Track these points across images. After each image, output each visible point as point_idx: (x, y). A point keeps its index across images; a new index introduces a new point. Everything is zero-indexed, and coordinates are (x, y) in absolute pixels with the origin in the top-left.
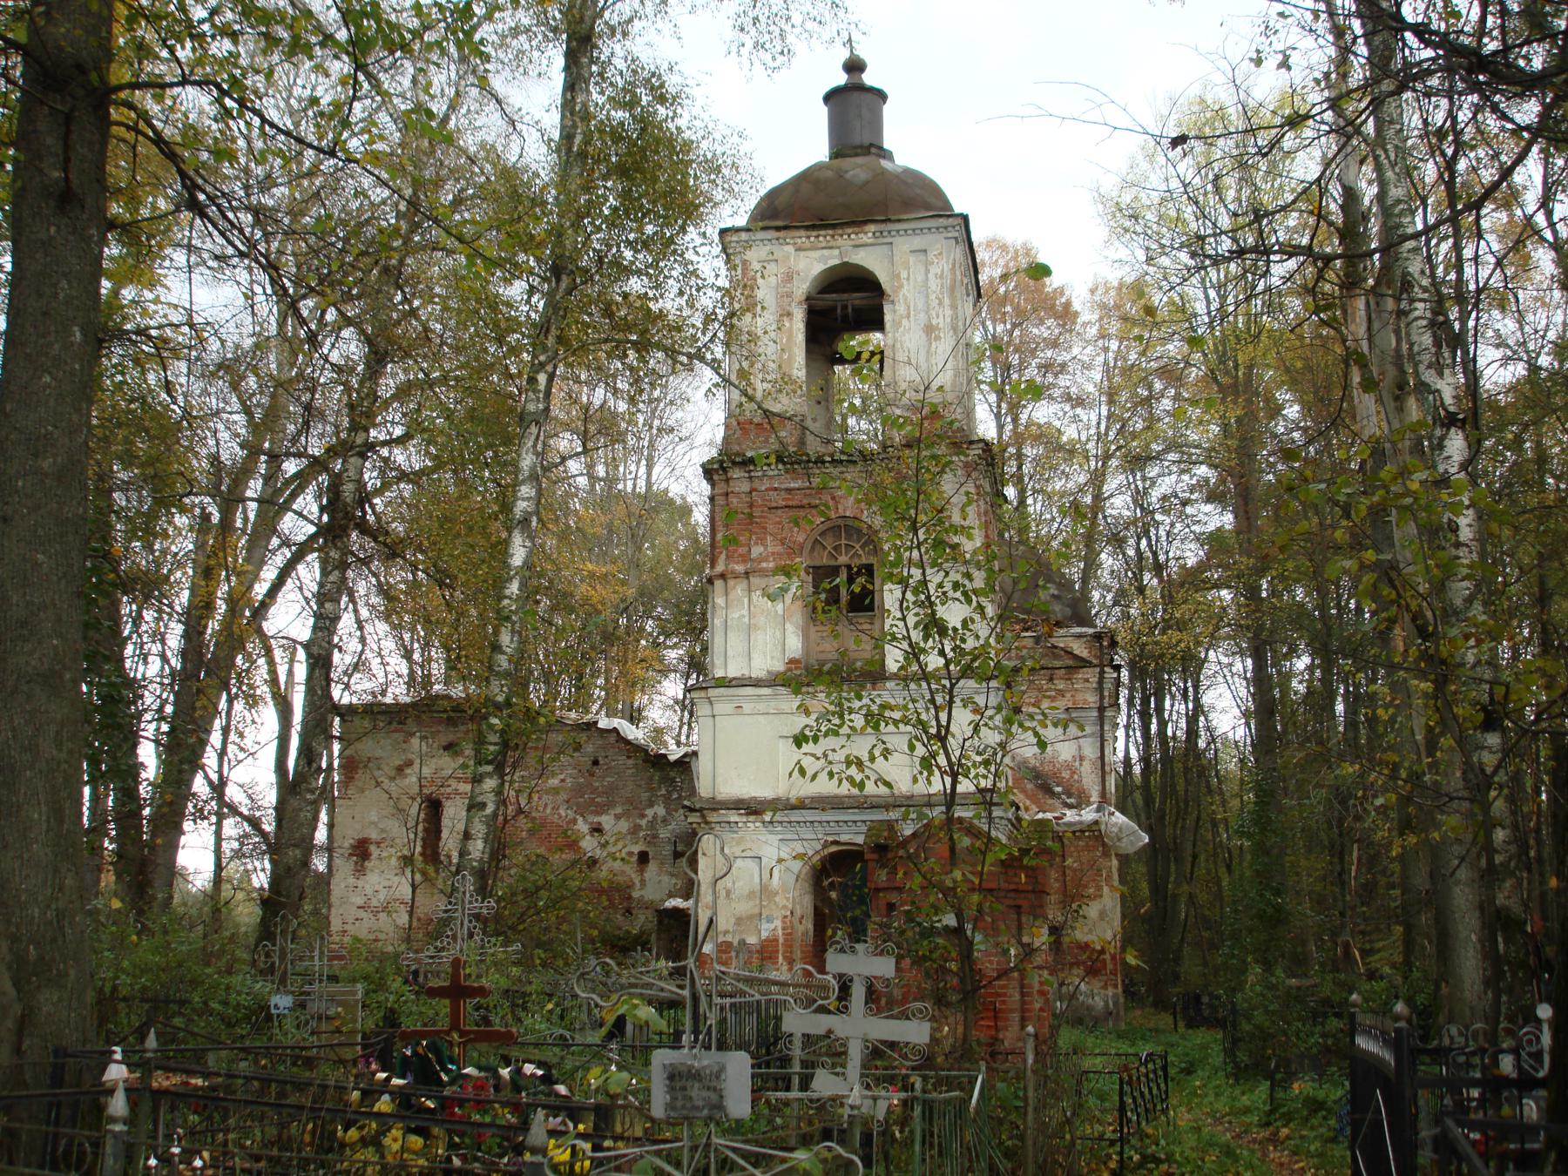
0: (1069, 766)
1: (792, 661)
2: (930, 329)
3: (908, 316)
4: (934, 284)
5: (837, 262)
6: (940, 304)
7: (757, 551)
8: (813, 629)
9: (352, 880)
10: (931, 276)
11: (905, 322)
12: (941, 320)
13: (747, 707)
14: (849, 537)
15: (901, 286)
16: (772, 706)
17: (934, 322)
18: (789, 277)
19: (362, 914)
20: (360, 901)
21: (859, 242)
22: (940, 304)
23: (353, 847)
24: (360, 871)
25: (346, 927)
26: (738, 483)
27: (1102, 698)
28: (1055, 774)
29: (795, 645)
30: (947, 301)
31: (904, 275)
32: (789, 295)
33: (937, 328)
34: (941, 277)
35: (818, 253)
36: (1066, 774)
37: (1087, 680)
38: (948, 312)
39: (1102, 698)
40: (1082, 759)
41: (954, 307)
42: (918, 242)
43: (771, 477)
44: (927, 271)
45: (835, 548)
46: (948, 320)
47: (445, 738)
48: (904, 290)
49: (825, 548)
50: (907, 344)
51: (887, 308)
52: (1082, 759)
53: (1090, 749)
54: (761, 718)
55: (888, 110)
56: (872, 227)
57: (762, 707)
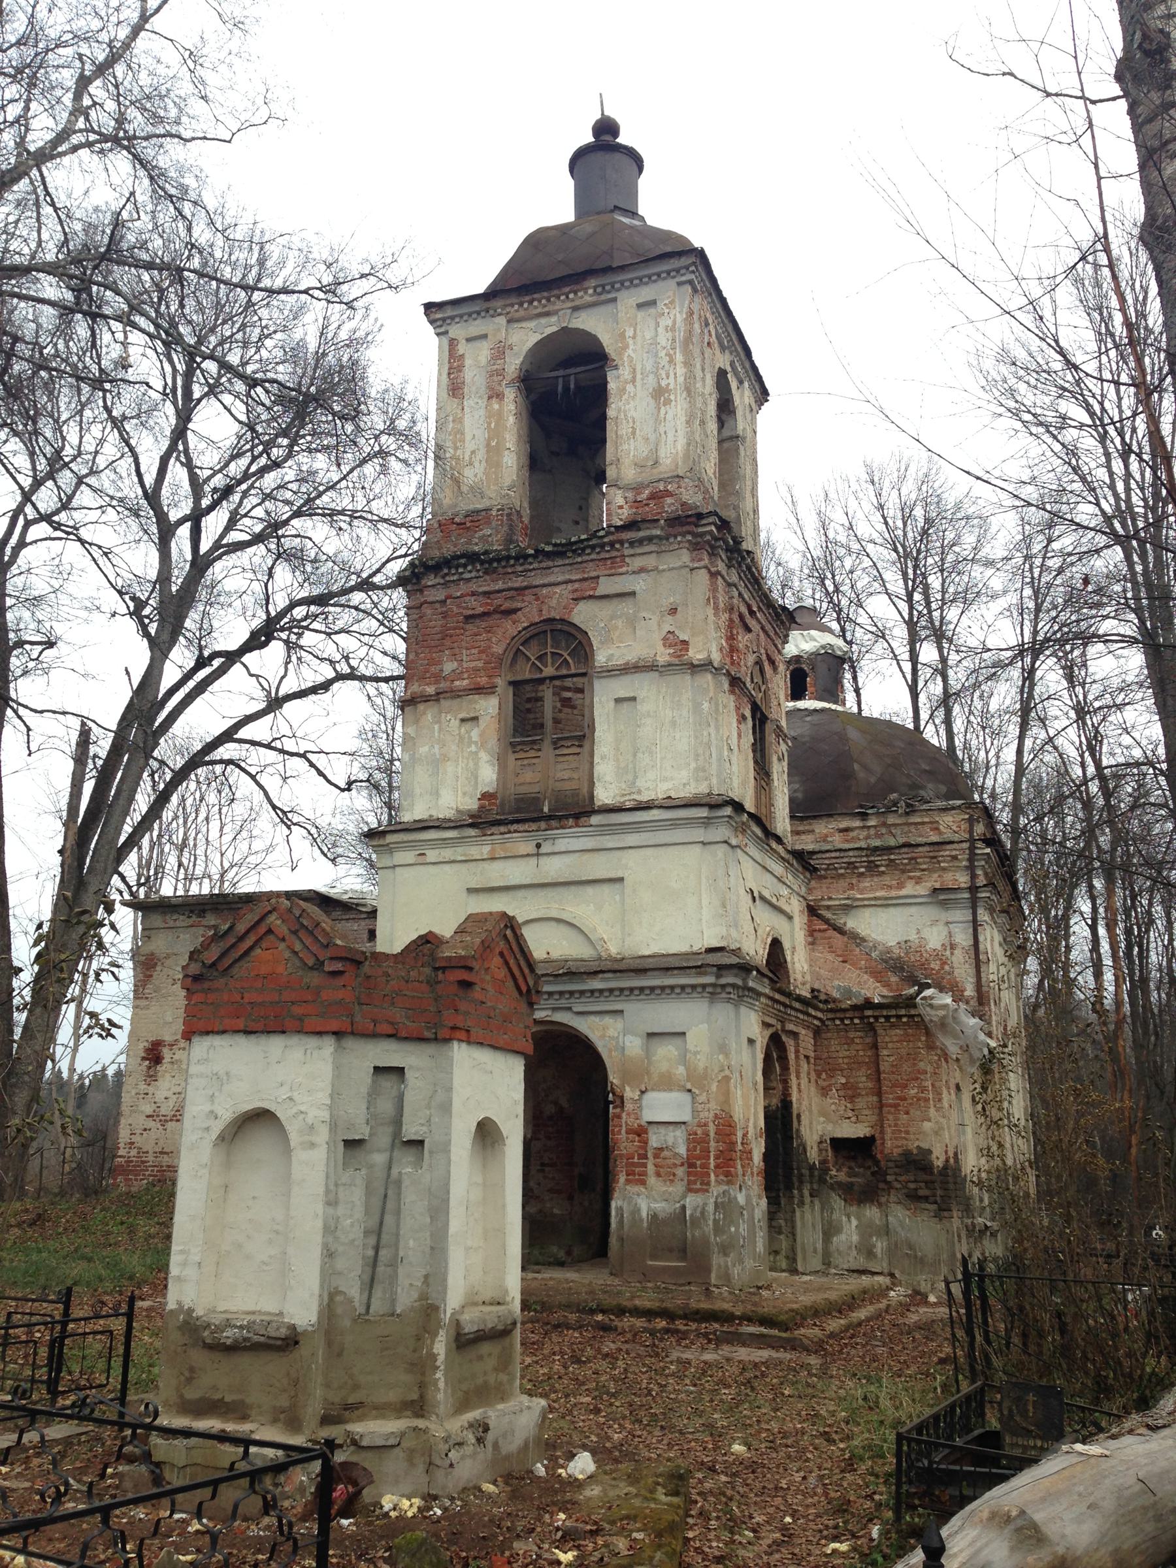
0: (937, 955)
1: (485, 796)
2: (660, 394)
3: (633, 381)
4: (663, 339)
5: (555, 329)
6: (671, 361)
7: (449, 667)
8: (512, 757)
9: (142, 1087)
10: (660, 330)
11: (630, 387)
12: (671, 380)
13: (432, 856)
14: (556, 644)
15: (626, 347)
16: (458, 853)
17: (663, 383)
18: (500, 352)
19: (150, 1124)
20: (148, 1109)
21: (577, 303)
22: (671, 361)
23: (147, 1050)
24: (151, 1077)
25: (135, 1139)
26: (433, 591)
27: (973, 877)
28: (923, 965)
29: (488, 776)
30: (679, 357)
31: (630, 332)
32: (501, 373)
33: (667, 390)
34: (673, 329)
35: (532, 324)
36: (935, 965)
37: (955, 858)
38: (681, 370)
39: (973, 877)
40: (953, 947)
41: (688, 364)
42: (645, 293)
43: (469, 580)
44: (658, 324)
45: (540, 658)
46: (681, 379)
47: (768, 1020)
48: (630, 352)
49: (528, 659)
50: (632, 413)
51: (611, 376)
52: (953, 947)
53: (963, 938)
54: (447, 867)
55: (644, 183)
56: (592, 282)
57: (448, 854)
